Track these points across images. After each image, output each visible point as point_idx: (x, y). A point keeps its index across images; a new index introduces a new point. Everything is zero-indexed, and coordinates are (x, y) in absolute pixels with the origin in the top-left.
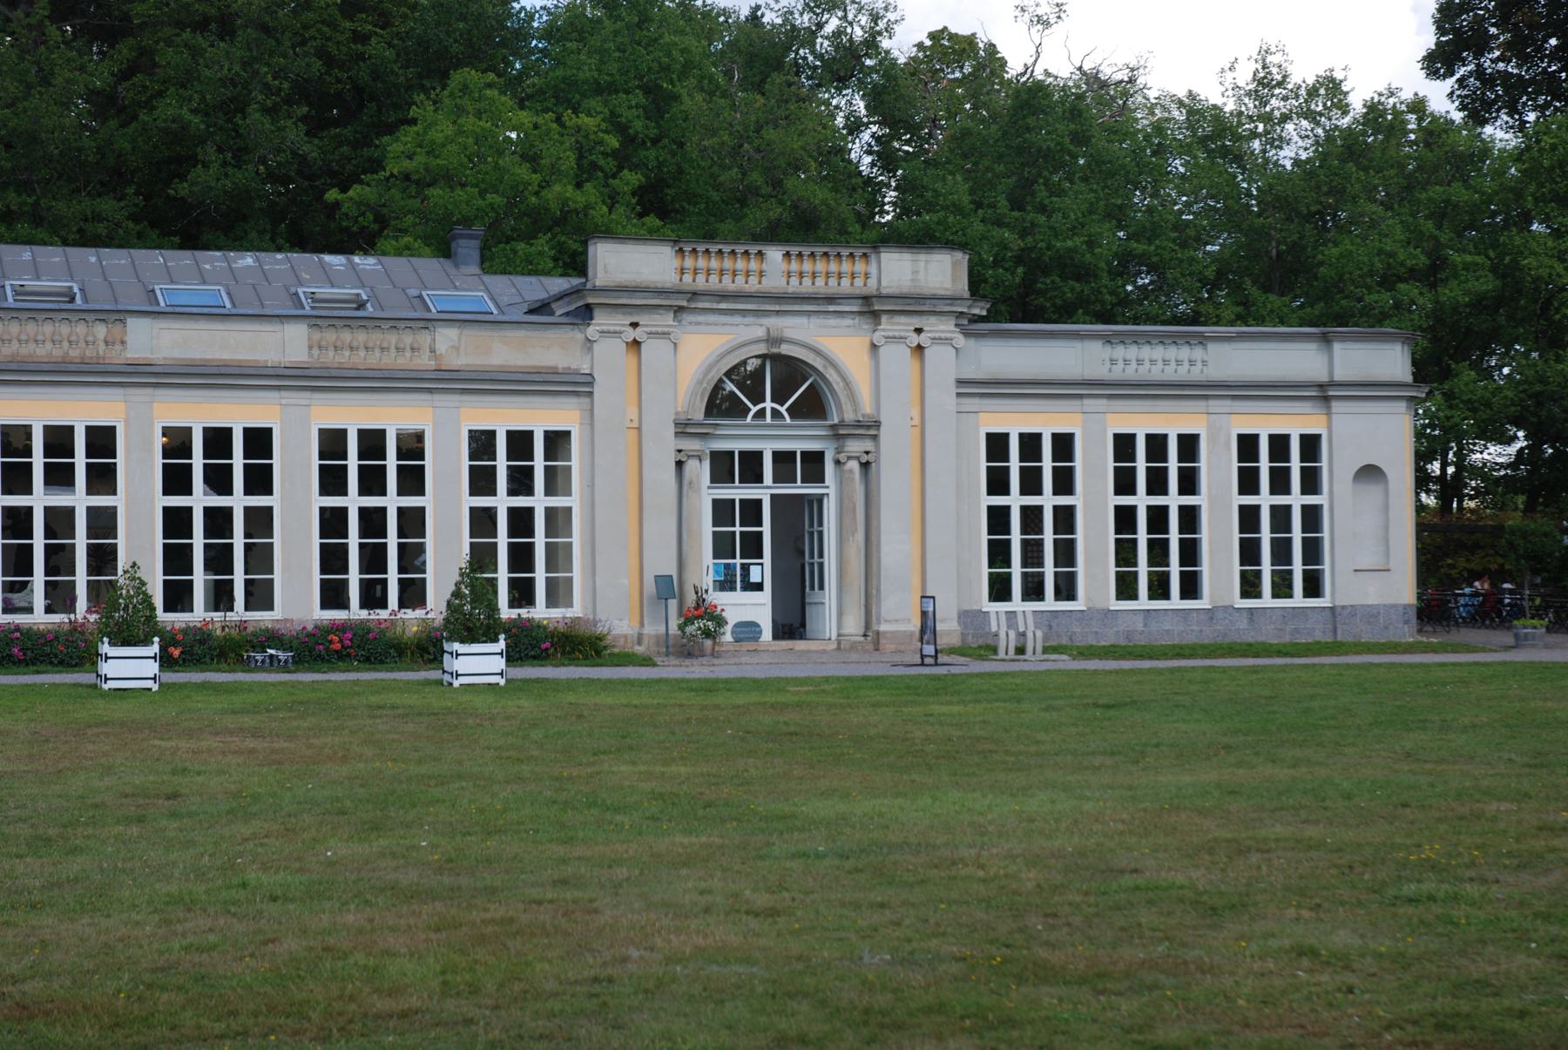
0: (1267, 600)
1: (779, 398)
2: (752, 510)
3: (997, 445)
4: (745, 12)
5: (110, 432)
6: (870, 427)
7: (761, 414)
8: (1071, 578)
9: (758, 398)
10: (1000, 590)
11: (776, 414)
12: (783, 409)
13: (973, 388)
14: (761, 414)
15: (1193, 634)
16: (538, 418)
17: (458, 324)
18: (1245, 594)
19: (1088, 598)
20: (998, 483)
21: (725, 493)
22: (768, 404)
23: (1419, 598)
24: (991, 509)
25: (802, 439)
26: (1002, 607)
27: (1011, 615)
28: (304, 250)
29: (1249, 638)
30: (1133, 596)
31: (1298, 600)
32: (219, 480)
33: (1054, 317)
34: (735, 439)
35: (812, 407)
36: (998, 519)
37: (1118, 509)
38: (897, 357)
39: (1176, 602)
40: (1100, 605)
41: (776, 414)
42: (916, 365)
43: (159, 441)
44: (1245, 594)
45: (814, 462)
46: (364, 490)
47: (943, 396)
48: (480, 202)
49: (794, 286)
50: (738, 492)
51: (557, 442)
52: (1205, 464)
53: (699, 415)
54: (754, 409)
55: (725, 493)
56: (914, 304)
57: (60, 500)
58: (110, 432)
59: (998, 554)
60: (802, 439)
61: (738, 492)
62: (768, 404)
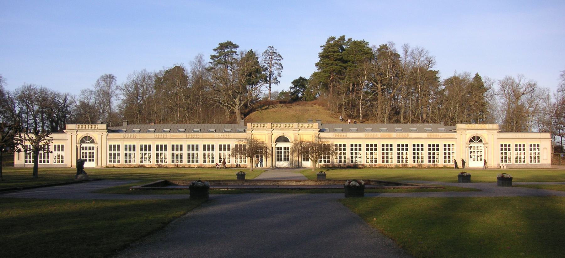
0: (518, 163)
1: (477, 140)
2: (86, 153)
3: (502, 146)
4: (473, 76)
5: (438, 145)
7: (475, 142)
9: (87, 141)
10: (502, 161)
11: (89, 142)
12: (89, 142)
14: (475, 142)
15: (524, 167)
18: (516, 162)
19: (541, 162)
20: (502, 150)
23: (551, 163)
24: (156, 153)
25: (92, 145)
27: (503, 164)
29: (531, 167)
30: (27, 162)
31: (46, 163)
32: (115, 150)
34: (84, 145)
35: (93, 142)
37: (444, 153)
39: (46, 163)
40: (513, 163)
41: (89, 142)
44: (516, 162)
45: (93, 148)
48: (553, 114)
50: (85, 151)
52: (526, 147)
53: (468, 142)
54: (86, 142)
57: (115, 152)
58: (438, 145)
60: (92, 145)
61: (85, 151)
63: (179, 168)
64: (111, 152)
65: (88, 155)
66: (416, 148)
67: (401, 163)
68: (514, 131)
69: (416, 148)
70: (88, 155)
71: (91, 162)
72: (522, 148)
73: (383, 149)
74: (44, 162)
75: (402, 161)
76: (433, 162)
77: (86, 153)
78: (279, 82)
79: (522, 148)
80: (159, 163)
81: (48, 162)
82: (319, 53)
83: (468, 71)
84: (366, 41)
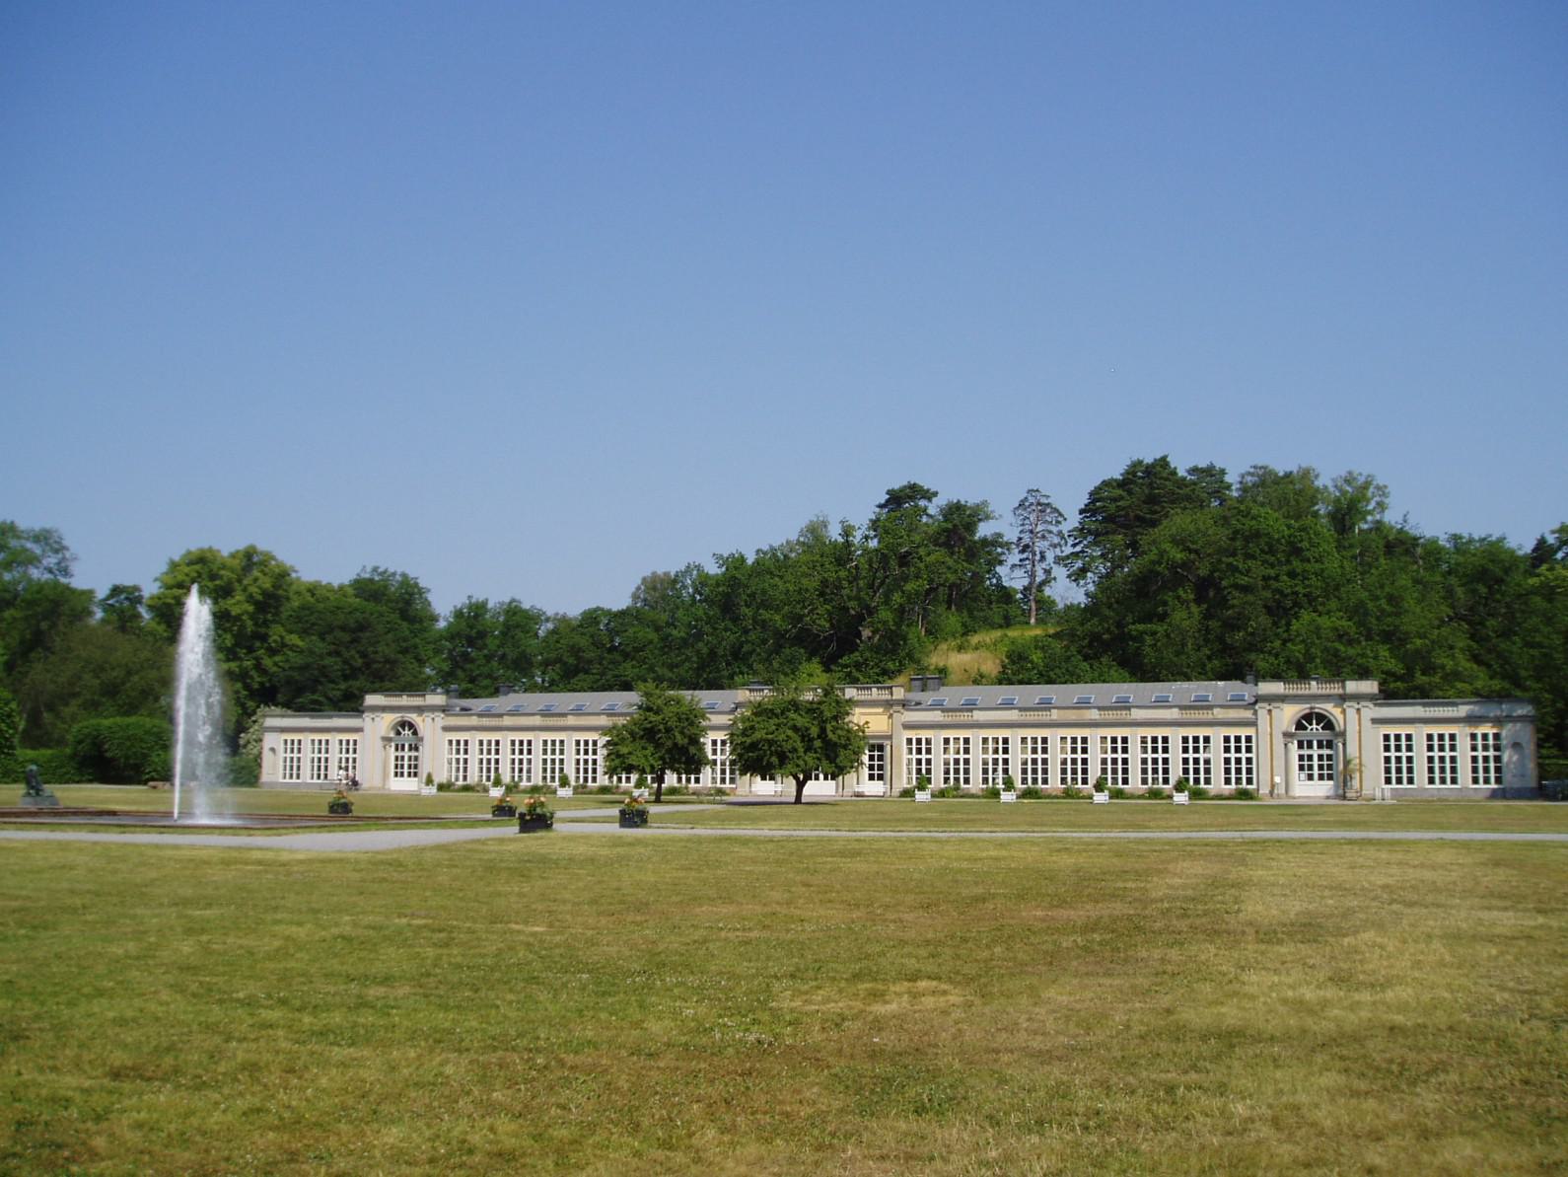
2: (1320, 757)
3: (1387, 738)
6: (1343, 734)
8: (1142, 742)
9: (1311, 724)
13: (446, 729)
16: (1243, 732)
17: (217, 831)
20: (1387, 748)
21: (1302, 752)
22: (1314, 726)
26: (1389, 786)
28: (1142, 680)
33: (77, 779)
36: (1387, 760)
38: (1351, 713)
42: (1357, 717)
43: (1139, 739)
46: (1066, 759)
47: (1366, 723)
49: (1320, 692)
50: (1305, 752)
51: (1249, 739)
55: (1302, 752)
56: (1357, 697)
59: (1388, 770)
61: (1305, 752)
62: (1314, 726)
63: (1072, 797)
64: (1249, 755)
65: (406, 763)
66: (1232, 744)
67: (1233, 786)
68: (140, 721)
69: (1232, 744)
70: (406, 763)
71: (413, 779)
72: (525, 747)
73: (1430, 748)
74: (1443, 781)
75: (1238, 781)
76: (1237, 783)
77: (1310, 758)
78: (1055, 579)
79: (525, 747)
80: (718, 785)
81: (1411, 781)
82: (1080, 514)
83: (668, 570)
84: (1218, 465)
